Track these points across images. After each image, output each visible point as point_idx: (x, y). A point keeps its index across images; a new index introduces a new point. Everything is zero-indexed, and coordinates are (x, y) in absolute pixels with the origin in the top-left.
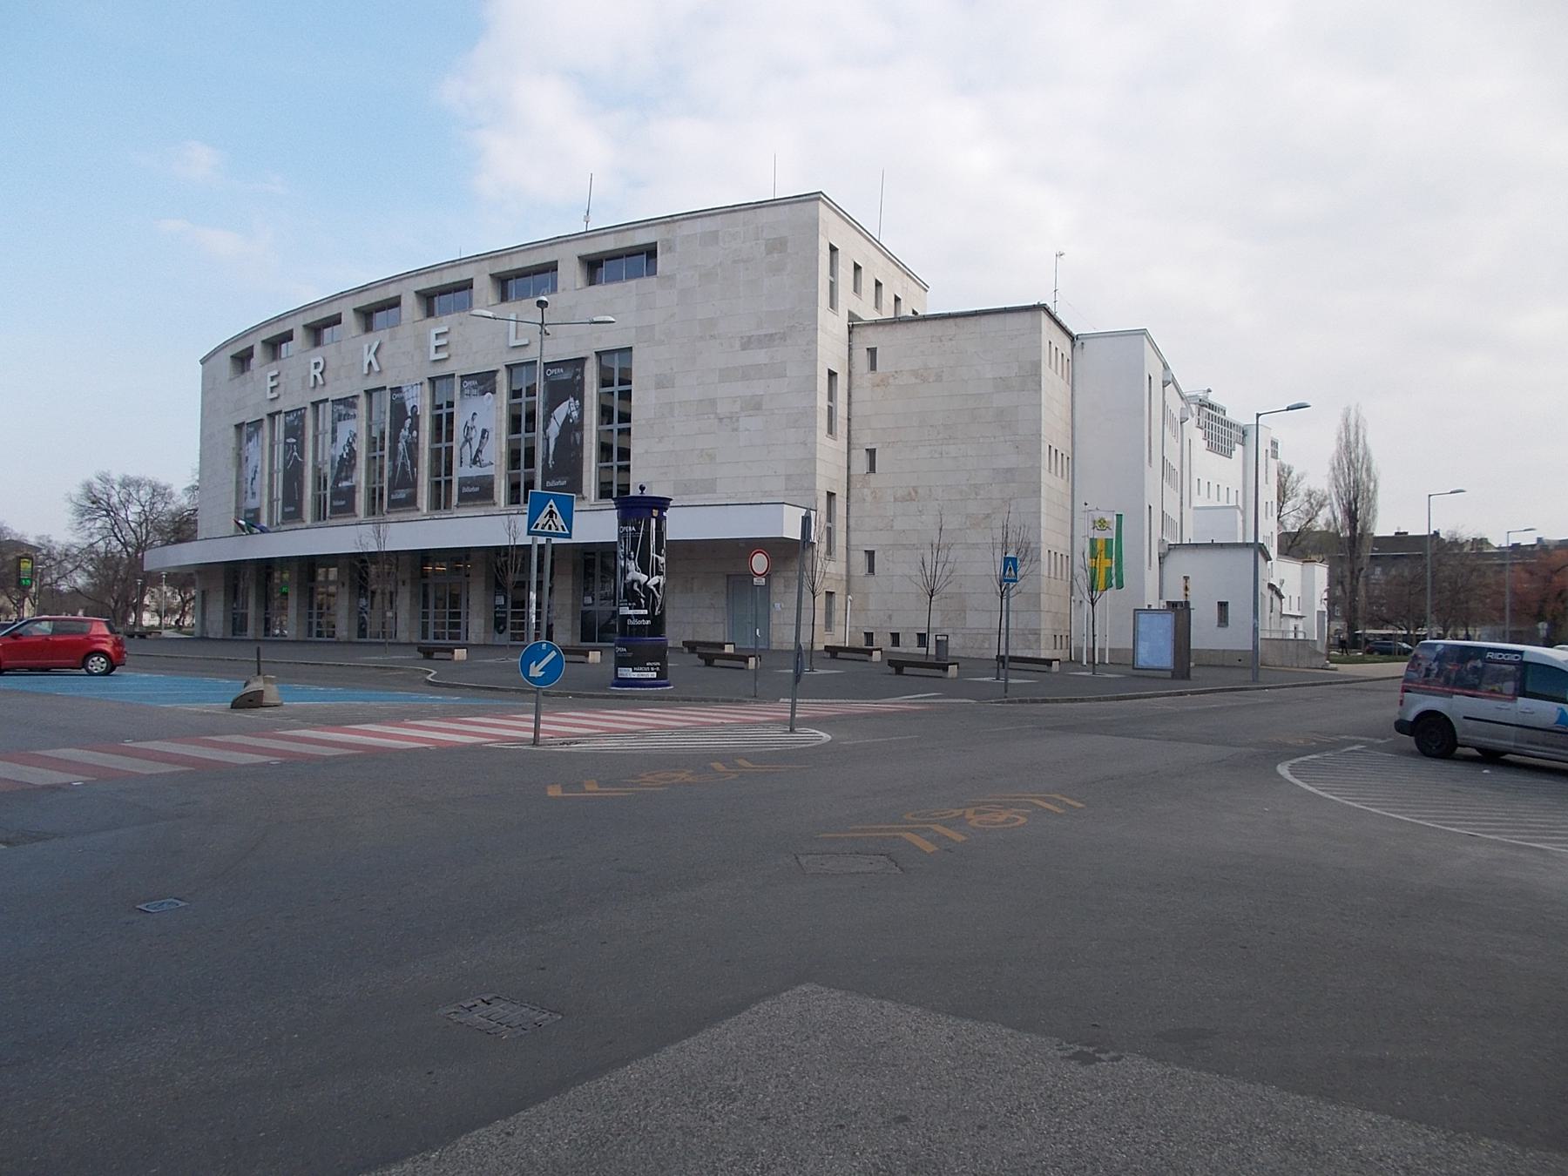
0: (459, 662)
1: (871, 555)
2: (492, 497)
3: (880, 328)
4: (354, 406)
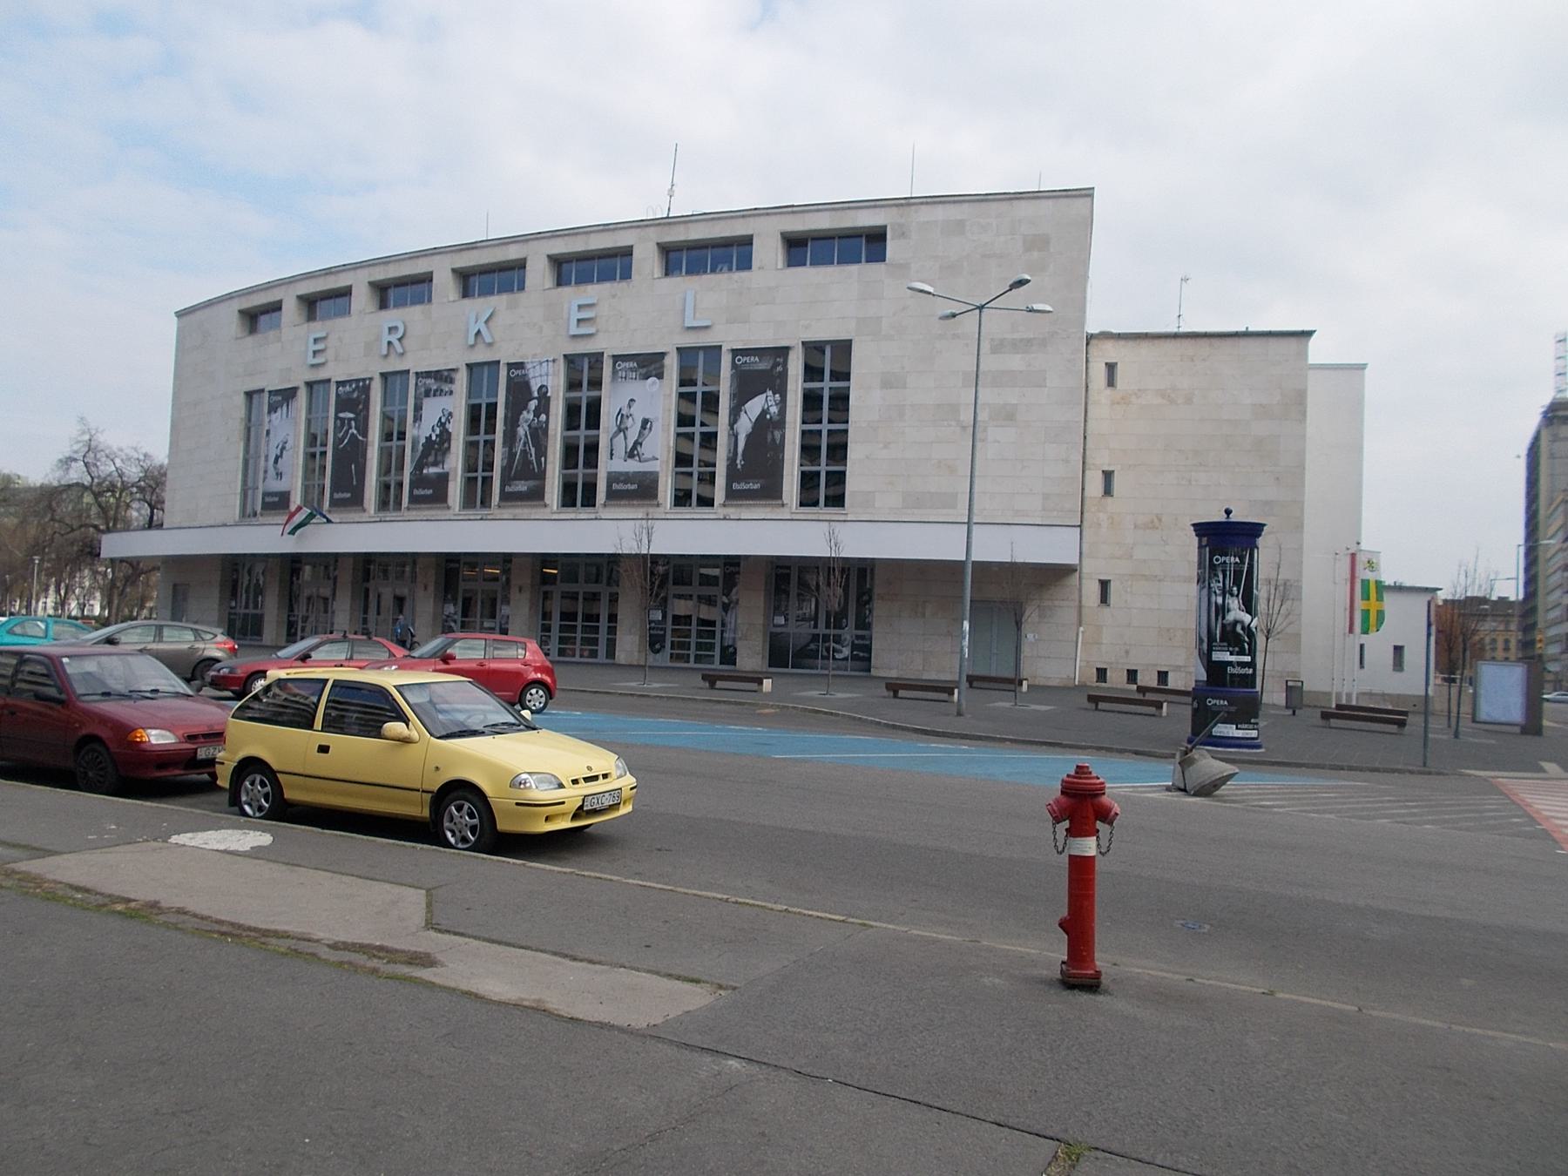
0: (767, 694)
1: (1104, 585)
2: (655, 496)
3: (1122, 343)
4: (452, 381)
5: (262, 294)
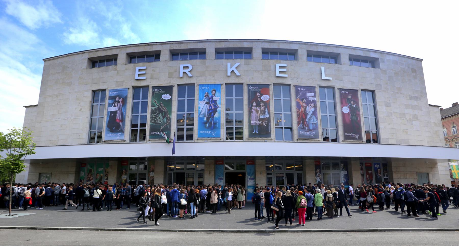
5: (104, 52)
